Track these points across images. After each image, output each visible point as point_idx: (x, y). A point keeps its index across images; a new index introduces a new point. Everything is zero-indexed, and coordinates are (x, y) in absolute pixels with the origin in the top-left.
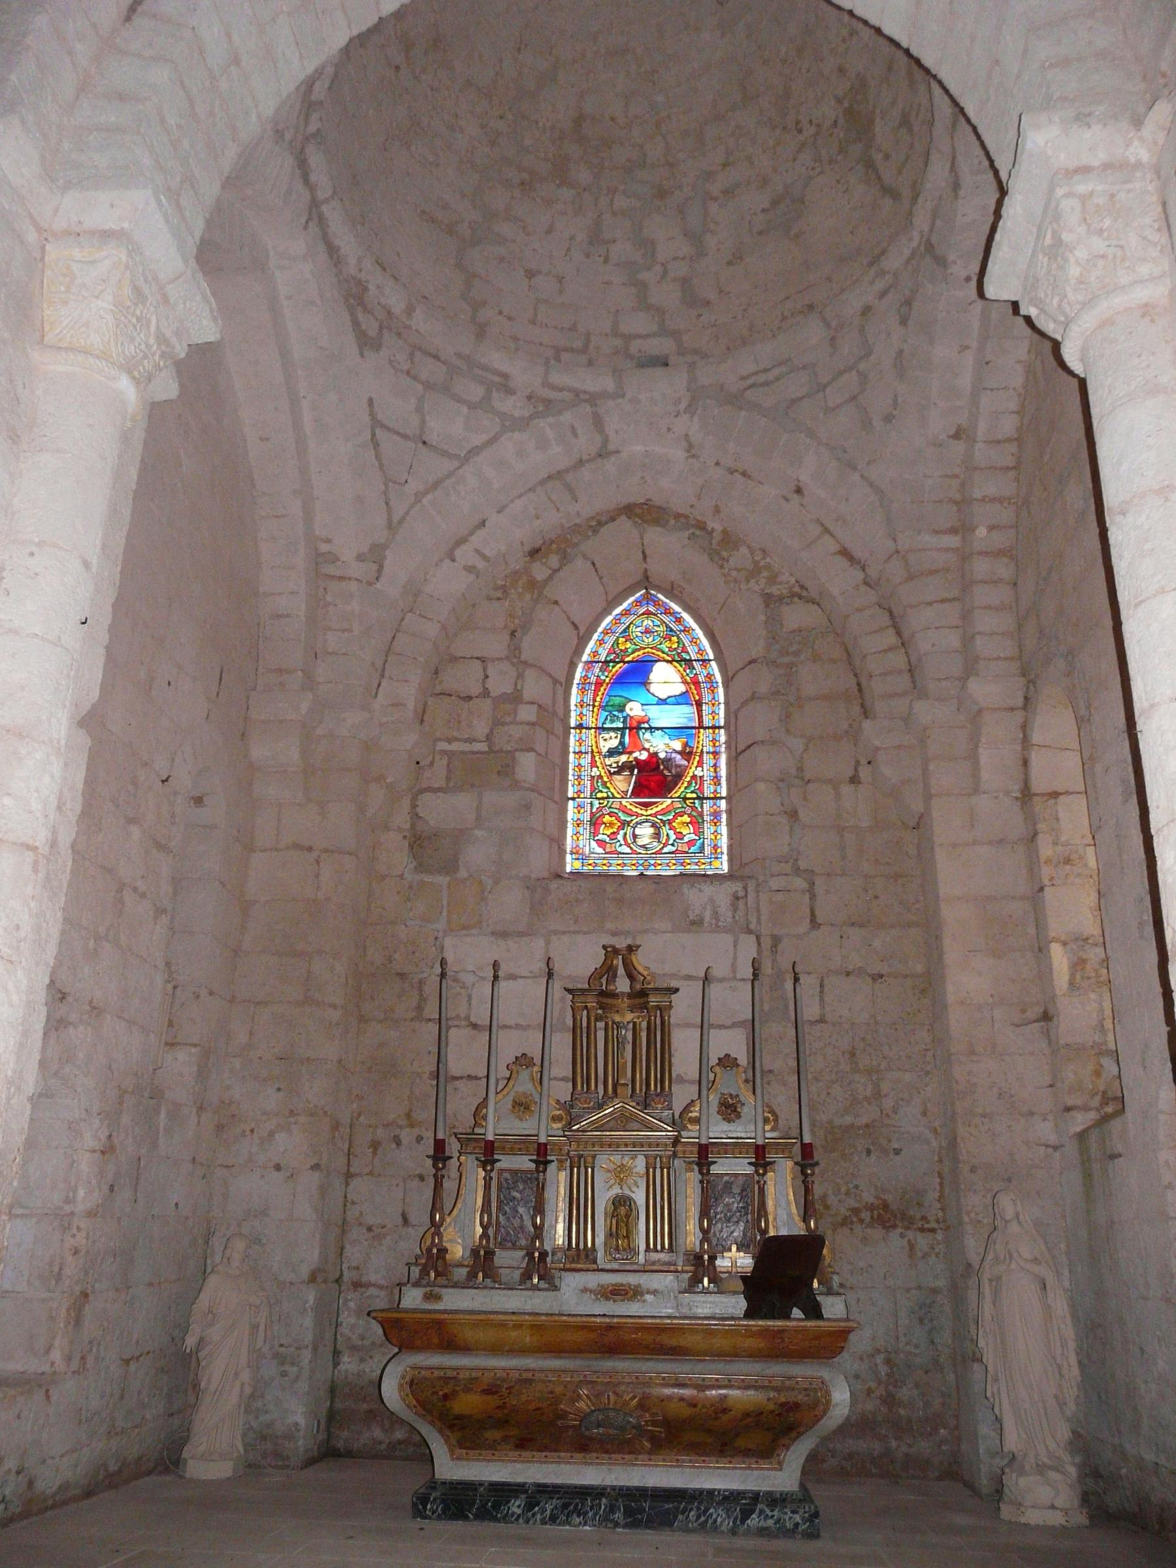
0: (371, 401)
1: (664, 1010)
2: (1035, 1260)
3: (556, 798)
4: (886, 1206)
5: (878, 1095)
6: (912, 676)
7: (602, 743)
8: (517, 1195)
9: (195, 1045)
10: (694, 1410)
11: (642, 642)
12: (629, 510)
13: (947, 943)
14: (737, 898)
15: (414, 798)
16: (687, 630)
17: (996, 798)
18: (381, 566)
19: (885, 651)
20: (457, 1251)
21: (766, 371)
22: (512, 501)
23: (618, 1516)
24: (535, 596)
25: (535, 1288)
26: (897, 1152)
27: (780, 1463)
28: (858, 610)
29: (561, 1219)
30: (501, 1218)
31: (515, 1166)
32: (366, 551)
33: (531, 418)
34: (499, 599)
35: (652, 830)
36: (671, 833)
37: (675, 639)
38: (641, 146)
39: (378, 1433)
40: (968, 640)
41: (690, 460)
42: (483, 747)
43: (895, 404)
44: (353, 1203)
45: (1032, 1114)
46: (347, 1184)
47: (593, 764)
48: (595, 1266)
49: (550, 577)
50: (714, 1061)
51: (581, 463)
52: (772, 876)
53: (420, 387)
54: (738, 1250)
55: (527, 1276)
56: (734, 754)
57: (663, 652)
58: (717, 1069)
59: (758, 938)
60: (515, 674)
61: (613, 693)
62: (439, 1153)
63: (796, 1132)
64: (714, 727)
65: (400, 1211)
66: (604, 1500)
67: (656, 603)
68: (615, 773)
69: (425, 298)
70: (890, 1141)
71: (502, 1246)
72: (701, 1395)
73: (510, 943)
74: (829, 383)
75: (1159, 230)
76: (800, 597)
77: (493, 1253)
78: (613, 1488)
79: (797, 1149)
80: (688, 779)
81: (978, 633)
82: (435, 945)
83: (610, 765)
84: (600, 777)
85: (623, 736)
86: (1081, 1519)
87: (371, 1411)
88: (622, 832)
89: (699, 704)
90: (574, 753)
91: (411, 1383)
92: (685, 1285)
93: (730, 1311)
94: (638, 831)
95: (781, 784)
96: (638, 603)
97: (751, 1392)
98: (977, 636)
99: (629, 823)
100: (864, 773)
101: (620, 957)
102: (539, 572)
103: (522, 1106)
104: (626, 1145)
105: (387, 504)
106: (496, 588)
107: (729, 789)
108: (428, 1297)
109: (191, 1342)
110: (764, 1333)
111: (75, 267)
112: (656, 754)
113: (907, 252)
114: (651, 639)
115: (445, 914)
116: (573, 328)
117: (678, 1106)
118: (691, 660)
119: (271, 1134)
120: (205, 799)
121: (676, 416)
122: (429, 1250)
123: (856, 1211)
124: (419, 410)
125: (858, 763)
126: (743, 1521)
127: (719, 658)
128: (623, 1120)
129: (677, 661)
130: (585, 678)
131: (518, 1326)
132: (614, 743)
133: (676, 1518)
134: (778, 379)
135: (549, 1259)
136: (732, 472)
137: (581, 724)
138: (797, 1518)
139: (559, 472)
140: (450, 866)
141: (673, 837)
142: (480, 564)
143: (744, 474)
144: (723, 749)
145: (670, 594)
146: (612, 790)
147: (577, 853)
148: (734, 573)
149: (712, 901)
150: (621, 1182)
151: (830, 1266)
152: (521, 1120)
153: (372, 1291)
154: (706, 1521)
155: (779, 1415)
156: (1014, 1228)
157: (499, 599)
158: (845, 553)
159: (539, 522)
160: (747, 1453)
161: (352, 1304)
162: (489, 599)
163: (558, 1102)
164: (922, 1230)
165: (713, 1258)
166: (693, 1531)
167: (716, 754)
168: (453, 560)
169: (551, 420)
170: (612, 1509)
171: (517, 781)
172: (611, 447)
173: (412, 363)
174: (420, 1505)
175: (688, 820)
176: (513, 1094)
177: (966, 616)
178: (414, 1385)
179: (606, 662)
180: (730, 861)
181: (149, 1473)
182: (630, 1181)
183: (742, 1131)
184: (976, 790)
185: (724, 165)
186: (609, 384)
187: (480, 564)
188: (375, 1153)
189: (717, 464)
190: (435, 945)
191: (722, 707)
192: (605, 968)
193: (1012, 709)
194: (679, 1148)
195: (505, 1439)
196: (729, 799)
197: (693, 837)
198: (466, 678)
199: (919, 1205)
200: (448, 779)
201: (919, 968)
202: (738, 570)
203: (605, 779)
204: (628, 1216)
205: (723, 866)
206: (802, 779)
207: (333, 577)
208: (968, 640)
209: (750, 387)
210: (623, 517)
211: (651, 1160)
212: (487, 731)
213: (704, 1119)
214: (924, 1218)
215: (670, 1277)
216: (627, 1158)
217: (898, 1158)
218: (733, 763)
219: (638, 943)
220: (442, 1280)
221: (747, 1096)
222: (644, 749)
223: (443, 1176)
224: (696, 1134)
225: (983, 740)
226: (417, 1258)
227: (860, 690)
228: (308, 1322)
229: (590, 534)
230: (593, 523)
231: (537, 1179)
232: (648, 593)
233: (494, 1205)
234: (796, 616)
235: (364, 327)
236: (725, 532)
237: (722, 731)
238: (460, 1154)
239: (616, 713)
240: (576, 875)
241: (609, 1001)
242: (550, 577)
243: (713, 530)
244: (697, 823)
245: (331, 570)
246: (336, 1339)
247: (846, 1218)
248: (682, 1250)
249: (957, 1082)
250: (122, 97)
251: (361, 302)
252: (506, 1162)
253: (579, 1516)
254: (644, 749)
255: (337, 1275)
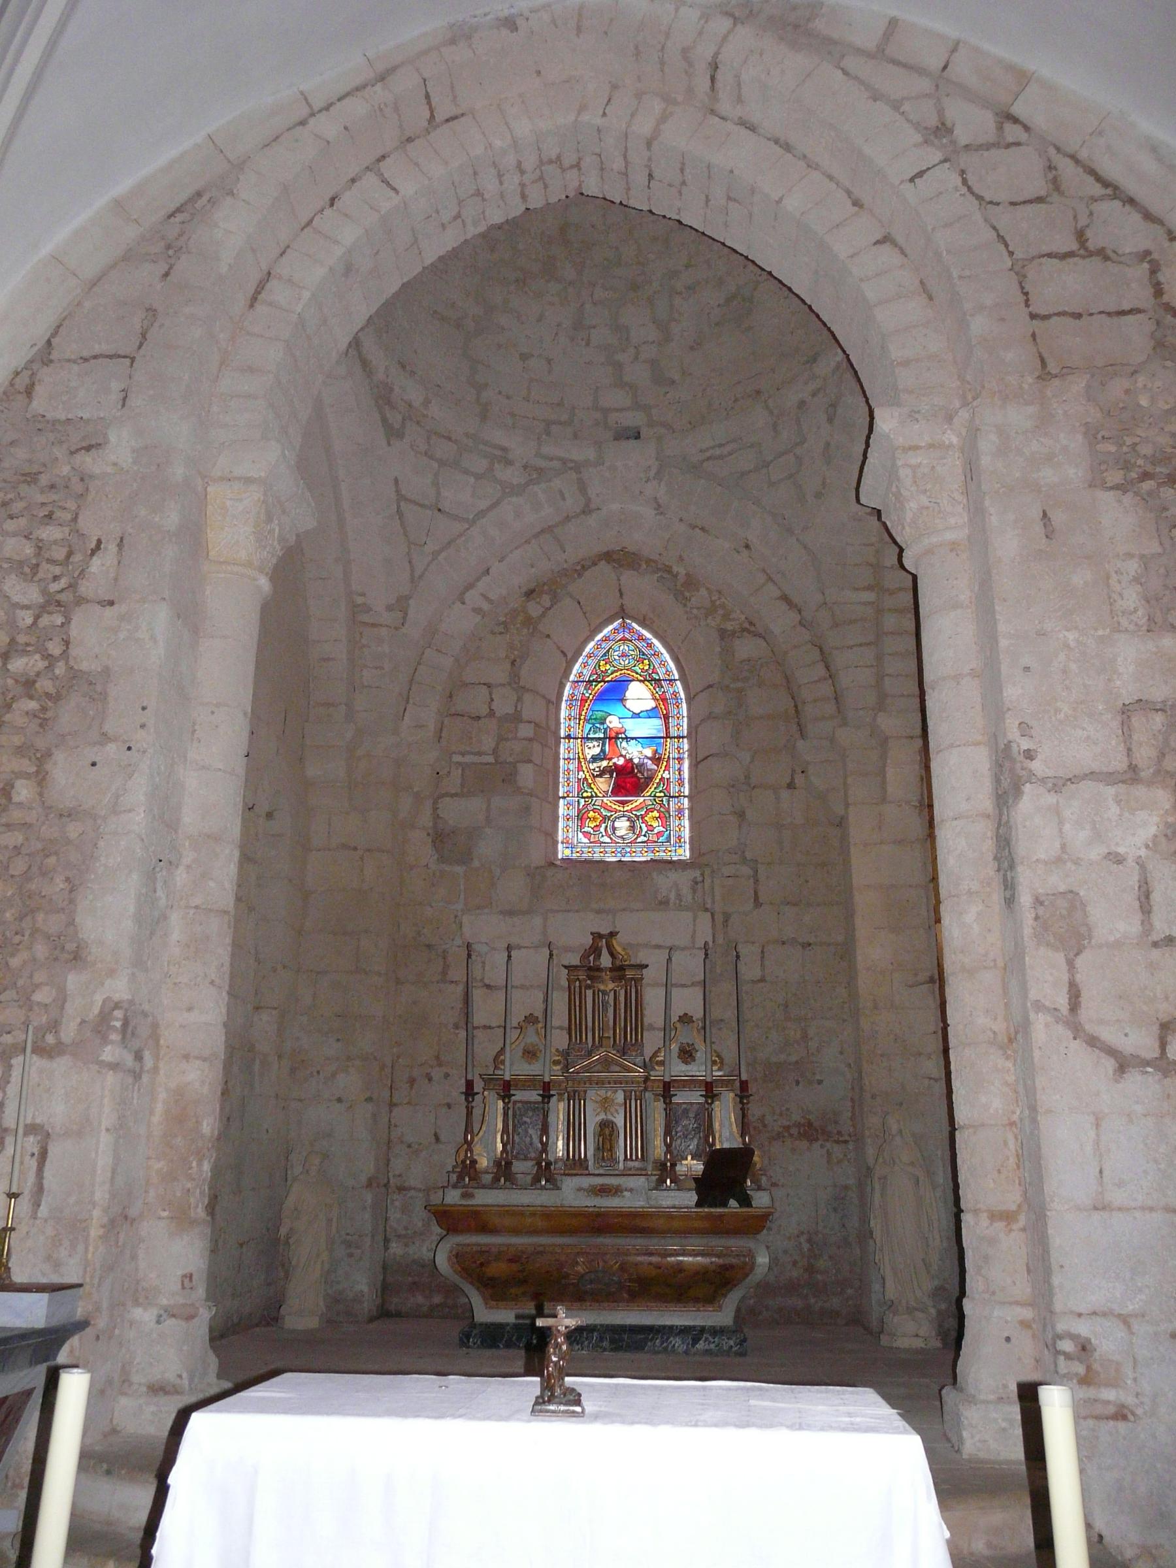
0: (396, 481)
1: (638, 981)
2: (912, 1164)
3: (550, 799)
4: (810, 1124)
5: (805, 1037)
6: (837, 702)
7: (587, 751)
8: (528, 1120)
9: (276, 1008)
10: (658, 1271)
11: (622, 656)
12: (608, 556)
13: (858, 921)
14: (696, 883)
15: (435, 802)
16: (657, 654)
17: (900, 806)
18: (406, 614)
19: (816, 682)
20: (484, 1163)
21: (720, 446)
22: (511, 552)
23: (605, 1344)
24: (531, 631)
25: (543, 1188)
26: (820, 1082)
27: (720, 1307)
28: (795, 647)
29: (561, 1138)
30: (516, 1138)
31: (525, 1099)
32: (394, 602)
33: (527, 484)
34: (501, 633)
35: (628, 824)
36: (643, 826)
37: (646, 662)
38: (617, 248)
39: (420, 1299)
40: (880, 678)
41: (658, 517)
42: (491, 759)
43: (824, 483)
44: (396, 1126)
45: (920, 1054)
46: (391, 1112)
47: (580, 768)
48: (587, 1172)
49: (543, 615)
50: (675, 1019)
51: (568, 519)
52: (725, 864)
53: (435, 465)
54: (692, 1159)
55: (536, 1179)
56: (694, 762)
57: (637, 673)
58: (678, 1025)
59: (713, 915)
60: (515, 698)
61: (596, 708)
62: (470, 1091)
63: (737, 1073)
64: (679, 737)
65: (433, 1132)
66: (595, 1334)
67: (631, 630)
68: (597, 776)
69: (438, 386)
70: (814, 1074)
71: (516, 1158)
72: (664, 1260)
73: (515, 919)
74: (772, 461)
75: (962, 493)
76: (749, 632)
77: (511, 1163)
78: (602, 1325)
79: (737, 1084)
80: (657, 781)
81: (887, 675)
82: (455, 922)
83: (594, 770)
84: (585, 779)
85: (604, 745)
86: (939, 1344)
87: (415, 1283)
88: (603, 826)
89: (666, 718)
90: (565, 759)
91: (457, 1256)
92: (653, 1185)
93: (686, 1203)
94: (617, 824)
95: (731, 790)
96: (616, 630)
97: (699, 1258)
98: (886, 678)
99: (609, 818)
100: (799, 780)
101: (604, 940)
102: (534, 610)
103: (530, 1054)
104: (609, 1083)
105: (410, 562)
106: (499, 624)
107: (690, 789)
108: (465, 1196)
109: (283, 1231)
110: (709, 1217)
111: (228, 503)
112: (631, 760)
113: (833, 364)
114: (627, 662)
115: (462, 896)
116: (560, 404)
117: (648, 1052)
118: (659, 680)
119: (334, 1075)
120: (275, 814)
121: (646, 482)
122: (463, 1162)
123: (787, 1128)
124: (436, 484)
125: (793, 771)
126: (693, 1345)
127: (683, 678)
128: (606, 1063)
129: (648, 681)
130: (572, 697)
131: (533, 1214)
132: (597, 751)
133: (646, 1344)
134: (730, 454)
135: (552, 1167)
136: (693, 527)
137: (569, 735)
138: (731, 1343)
139: (549, 527)
140: (465, 858)
141: (645, 829)
142: (486, 606)
143: (703, 529)
144: (686, 755)
145: (643, 624)
146: (595, 790)
147: (567, 842)
148: (695, 611)
149: (676, 884)
150: (605, 1110)
151: (760, 1170)
152: (530, 1064)
153: (412, 1193)
154: (667, 1346)
155: (719, 1273)
156: (898, 1139)
157: (501, 633)
158: (785, 598)
159: (533, 570)
160: (696, 1300)
161: (397, 1204)
162: (493, 633)
163: (557, 1050)
164: (838, 1142)
165: (673, 1165)
166: (659, 1352)
167: (680, 759)
168: (463, 603)
169: (543, 485)
170: (601, 1339)
171: (519, 788)
172: (593, 506)
173: (430, 445)
174: (464, 1340)
175: (657, 815)
176: (523, 1045)
177: (879, 658)
178: (458, 1257)
179: (590, 682)
180: (691, 849)
181: (257, 1325)
182: (612, 1110)
183: (697, 1070)
184: (884, 800)
185: (687, 267)
186: (590, 453)
187: (486, 606)
188: (411, 1088)
189: (681, 520)
190: (455, 922)
191: (685, 719)
192: (592, 950)
193: (912, 738)
194: (649, 1083)
195: (524, 1294)
196: (690, 797)
197: (661, 829)
198: (476, 702)
199: (836, 1122)
200: (462, 786)
201: (840, 938)
202: (698, 608)
203: (590, 781)
204: (611, 1135)
205: (684, 853)
206: (749, 785)
207: (365, 624)
208: (880, 678)
209: (708, 459)
210: (603, 562)
211: (628, 1094)
212: (493, 745)
213: (667, 1063)
214: (839, 1133)
215: (643, 1179)
216: (609, 1093)
217: (820, 1086)
218: (694, 782)
219: (617, 930)
220: (473, 1183)
221: (700, 1046)
222: (621, 756)
223: (472, 1107)
224: (662, 1073)
225: (889, 761)
226: (454, 1167)
227: (797, 711)
228: (367, 1216)
229: (576, 576)
230: (579, 568)
231: (543, 1109)
232: (624, 626)
233: (511, 1128)
234: (746, 648)
235: (390, 422)
236: (687, 575)
237: (685, 740)
238: (484, 1089)
239: (598, 725)
240: (567, 860)
241: (596, 974)
242: (543, 615)
243: (678, 573)
244: (664, 818)
245: (365, 618)
246: (385, 1231)
247: (779, 1134)
248: (652, 1160)
249: (863, 1031)
250: (251, 370)
251: (389, 403)
252: (519, 1095)
253: (578, 1344)
254: (621, 756)
255: (386, 1181)
